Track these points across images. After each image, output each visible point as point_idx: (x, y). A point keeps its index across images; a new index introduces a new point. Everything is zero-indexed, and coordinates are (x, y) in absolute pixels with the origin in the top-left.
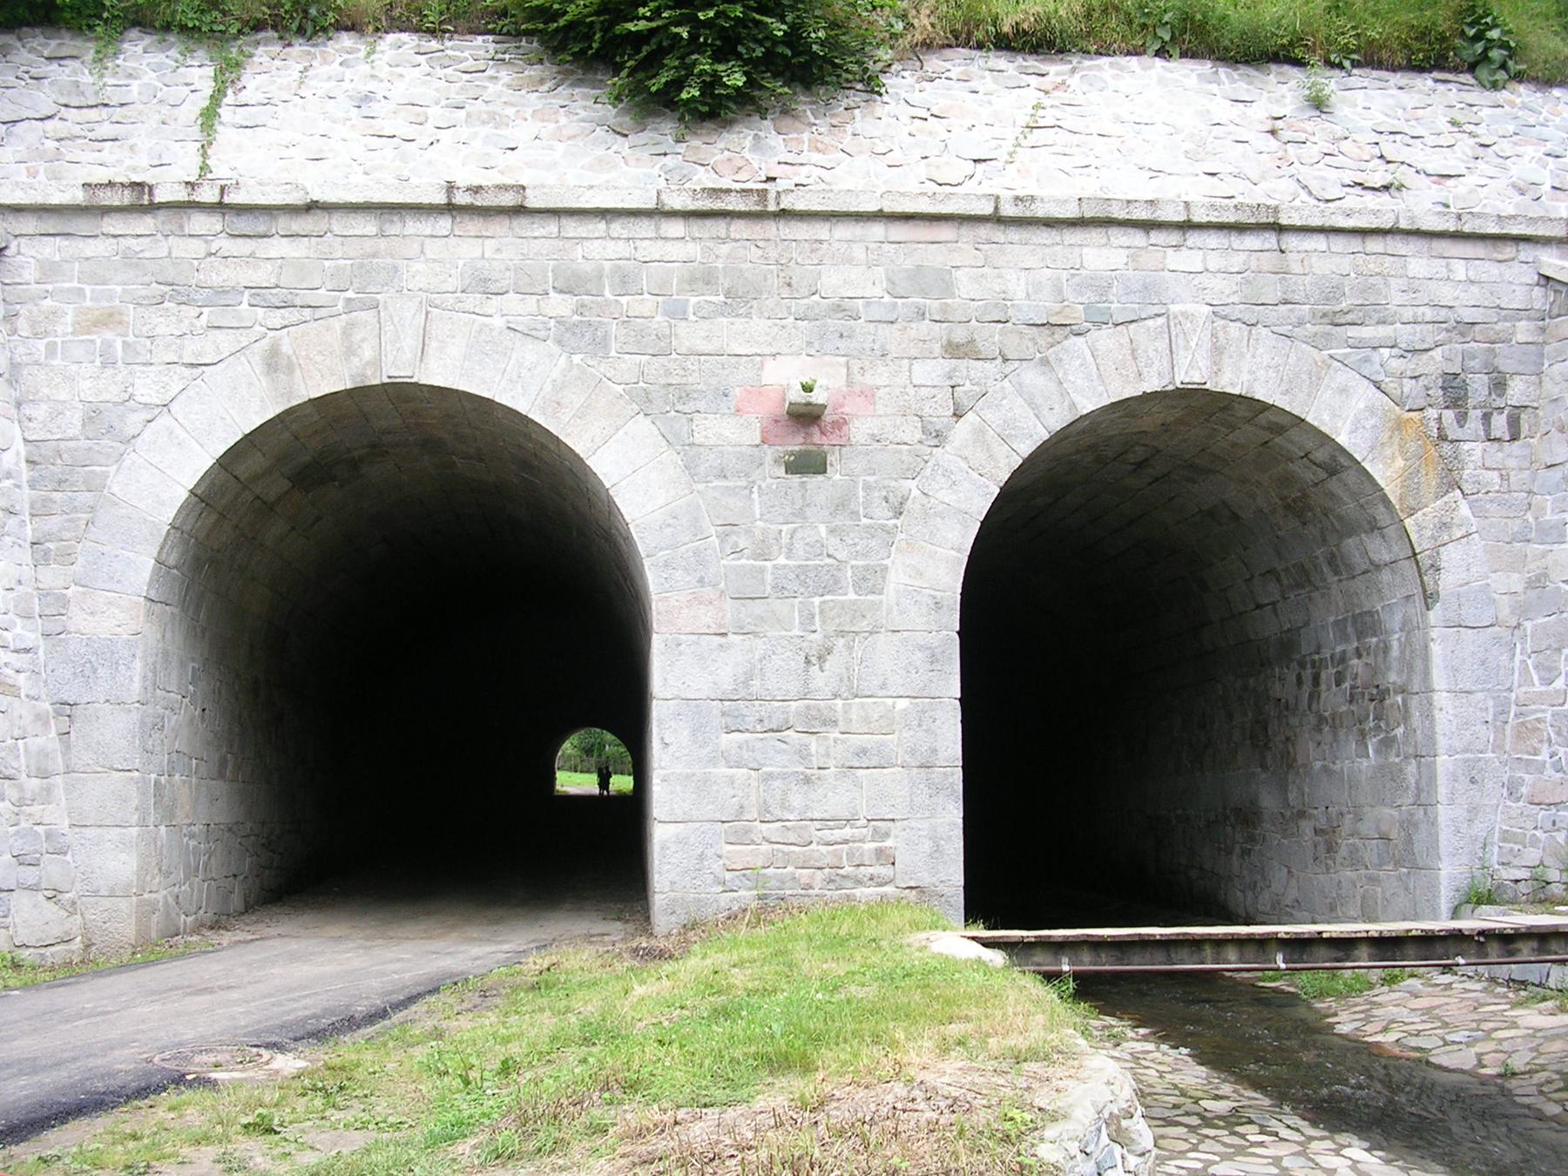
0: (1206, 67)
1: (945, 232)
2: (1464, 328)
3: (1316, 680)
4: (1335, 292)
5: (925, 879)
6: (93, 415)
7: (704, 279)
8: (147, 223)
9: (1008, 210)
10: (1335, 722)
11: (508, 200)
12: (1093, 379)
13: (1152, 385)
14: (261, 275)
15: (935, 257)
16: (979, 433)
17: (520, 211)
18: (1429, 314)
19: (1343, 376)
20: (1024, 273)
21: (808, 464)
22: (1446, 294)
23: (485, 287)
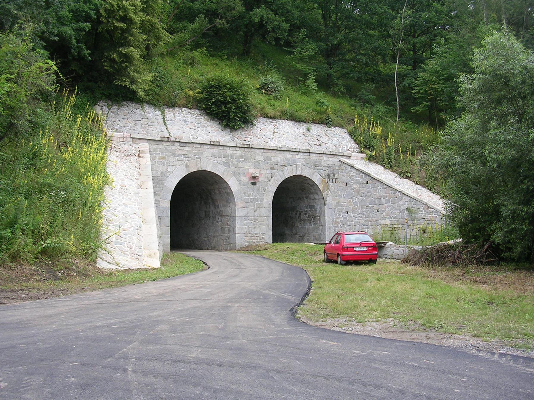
0: (293, 122)
1: (270, 151)
2: (330, 167)
3: (300, 214)
4: (316, 162)
5: (268, 241)
6: (162, 173)
7: (241, 157)
8: (169, 143)
9: (279, 149)
10: (304, 220)
11: (218, 144)
12: (288, 173)
13: (294, 174)
14: (185, 153)
15: (269, 155)
16: (274, 180)
17: (219, 145)
18: (326, 165)
19: (317, 174)
20: (279, 158)
21: (254, 184)
22: (328, 163)
23: (214, 156)
